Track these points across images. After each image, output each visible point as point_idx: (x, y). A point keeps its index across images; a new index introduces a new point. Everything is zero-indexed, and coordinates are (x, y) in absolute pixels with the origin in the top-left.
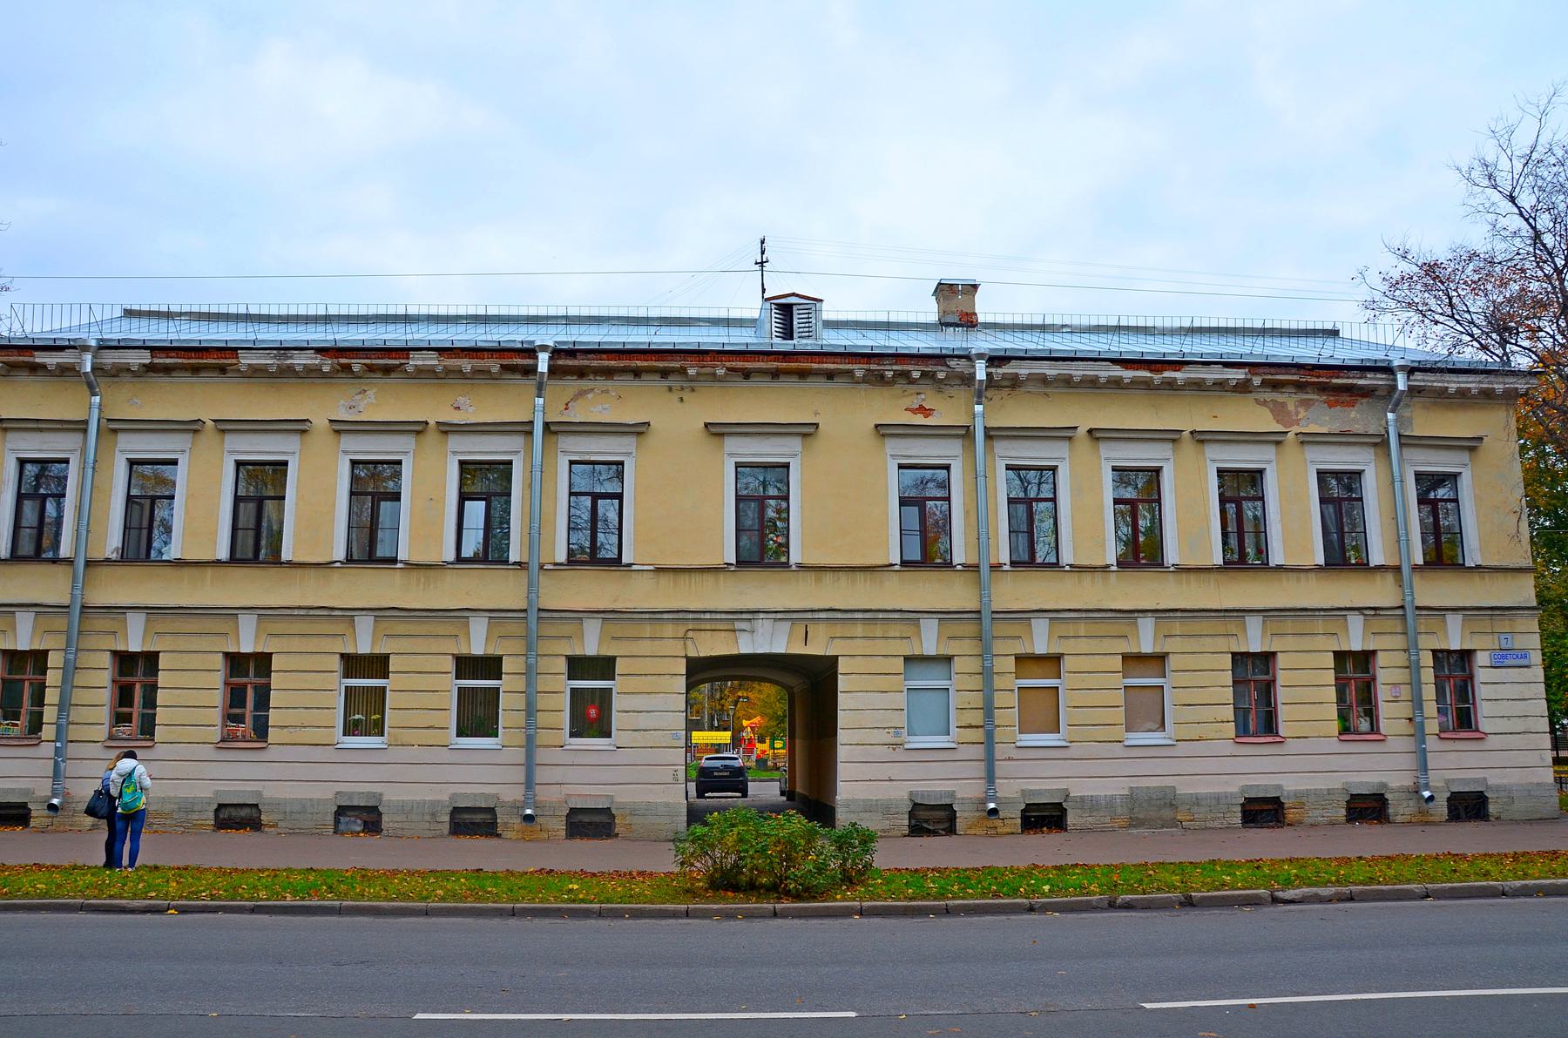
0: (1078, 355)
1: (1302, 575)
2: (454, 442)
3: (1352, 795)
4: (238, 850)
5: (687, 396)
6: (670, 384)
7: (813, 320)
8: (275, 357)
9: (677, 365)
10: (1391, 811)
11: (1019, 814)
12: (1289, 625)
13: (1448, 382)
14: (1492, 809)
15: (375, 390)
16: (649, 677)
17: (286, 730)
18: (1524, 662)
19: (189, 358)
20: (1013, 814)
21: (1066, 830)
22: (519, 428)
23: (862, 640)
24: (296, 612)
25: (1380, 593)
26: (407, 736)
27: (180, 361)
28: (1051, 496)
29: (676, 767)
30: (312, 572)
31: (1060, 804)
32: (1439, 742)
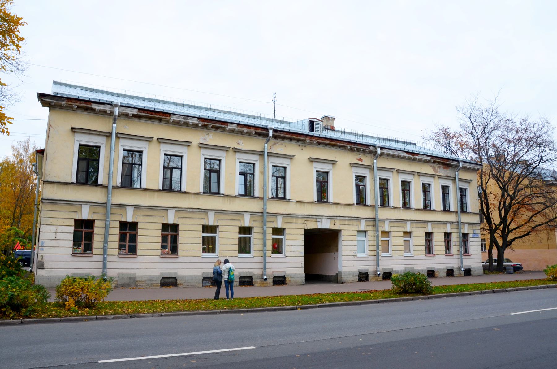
1: (438, 212)
4: (169, 294)
6: (300, 144)
7: (320, 127)
8: (183, 119)
9: (304, 139)
10: (454, 273)
12: (436, 225)
14: (472, 273)
15: (212, 134)
16: (294, 235)
17: (185, 251)
18: (477, 237)
22: (259, 153)
24: (189, 210)
25: (452, 218)
27: (148, 115)
28: (283, 175)
29: (302, 263)
30: (193, 196)
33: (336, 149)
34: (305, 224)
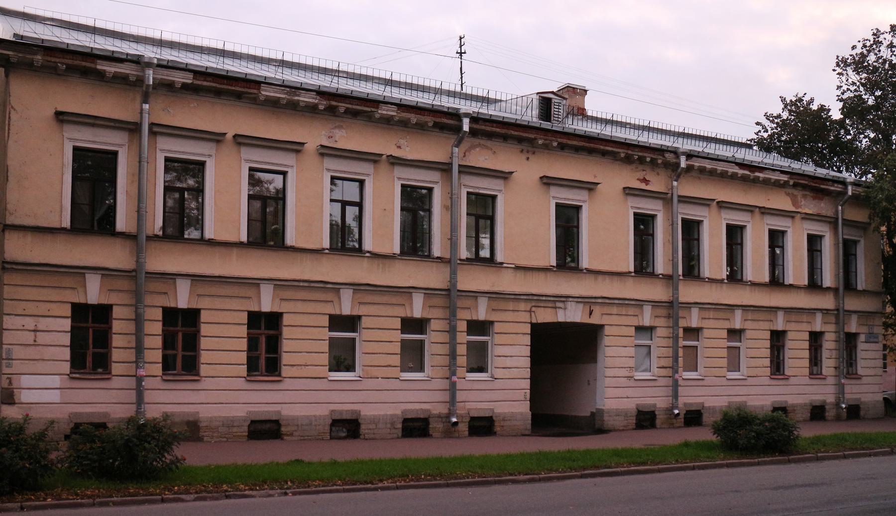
2: (399, 172)
5: (531, 157)
6: (523, 147)
9: (532, 136)
14: (862, 413)
19: (221, 84)
23: (617, 316)
24: (301, 284)
26: (375, 372)
28: (357, 200)
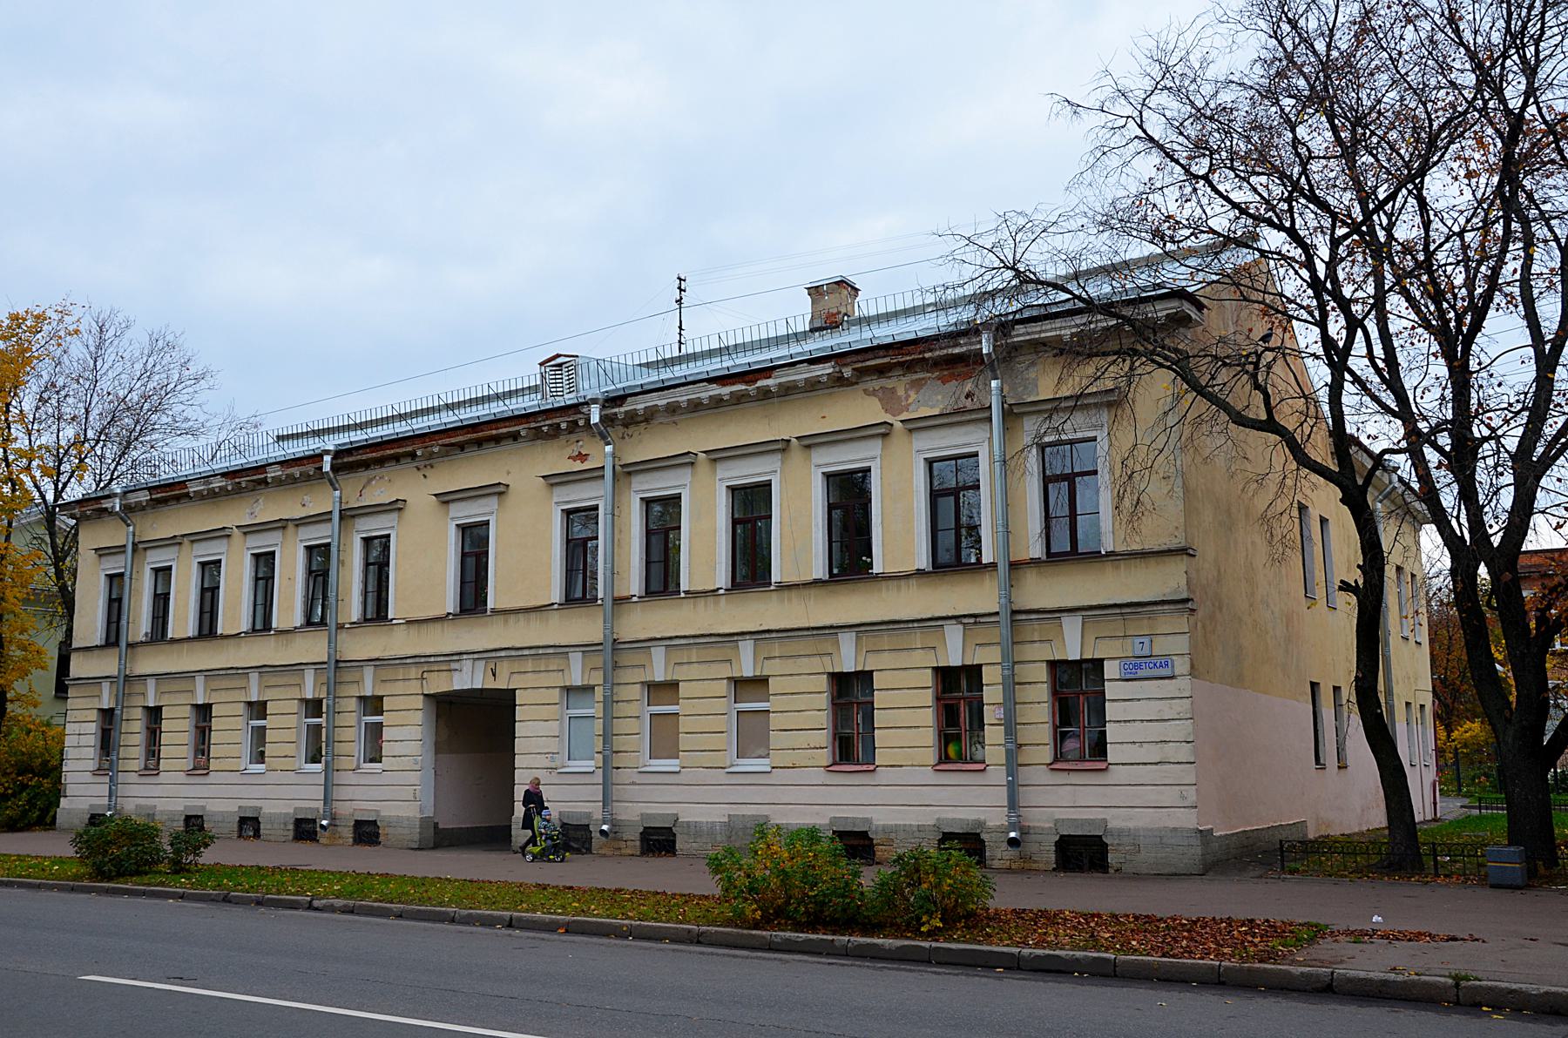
0: (689, 379)
1: (903, 582)
3: (944, 833)
5: (428, 472)
9: (409, 449)
11: (638, 835)
12: (886, 641)
13: (1060, 328)
14: (1112, 858)
20: (633, 835)
21: (675, 855)
24: (221, 672)
31: (671, 828)
32: (1049, 773)
33: (490, 451)
34: (424, 682)
